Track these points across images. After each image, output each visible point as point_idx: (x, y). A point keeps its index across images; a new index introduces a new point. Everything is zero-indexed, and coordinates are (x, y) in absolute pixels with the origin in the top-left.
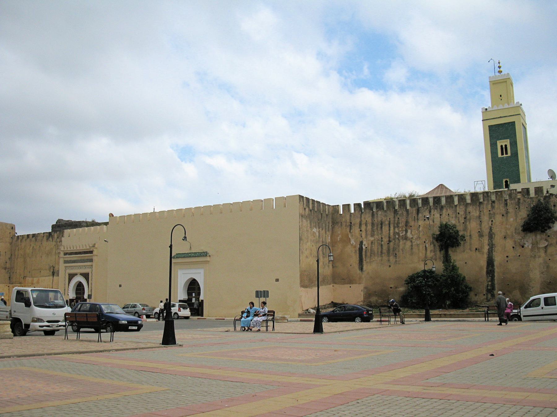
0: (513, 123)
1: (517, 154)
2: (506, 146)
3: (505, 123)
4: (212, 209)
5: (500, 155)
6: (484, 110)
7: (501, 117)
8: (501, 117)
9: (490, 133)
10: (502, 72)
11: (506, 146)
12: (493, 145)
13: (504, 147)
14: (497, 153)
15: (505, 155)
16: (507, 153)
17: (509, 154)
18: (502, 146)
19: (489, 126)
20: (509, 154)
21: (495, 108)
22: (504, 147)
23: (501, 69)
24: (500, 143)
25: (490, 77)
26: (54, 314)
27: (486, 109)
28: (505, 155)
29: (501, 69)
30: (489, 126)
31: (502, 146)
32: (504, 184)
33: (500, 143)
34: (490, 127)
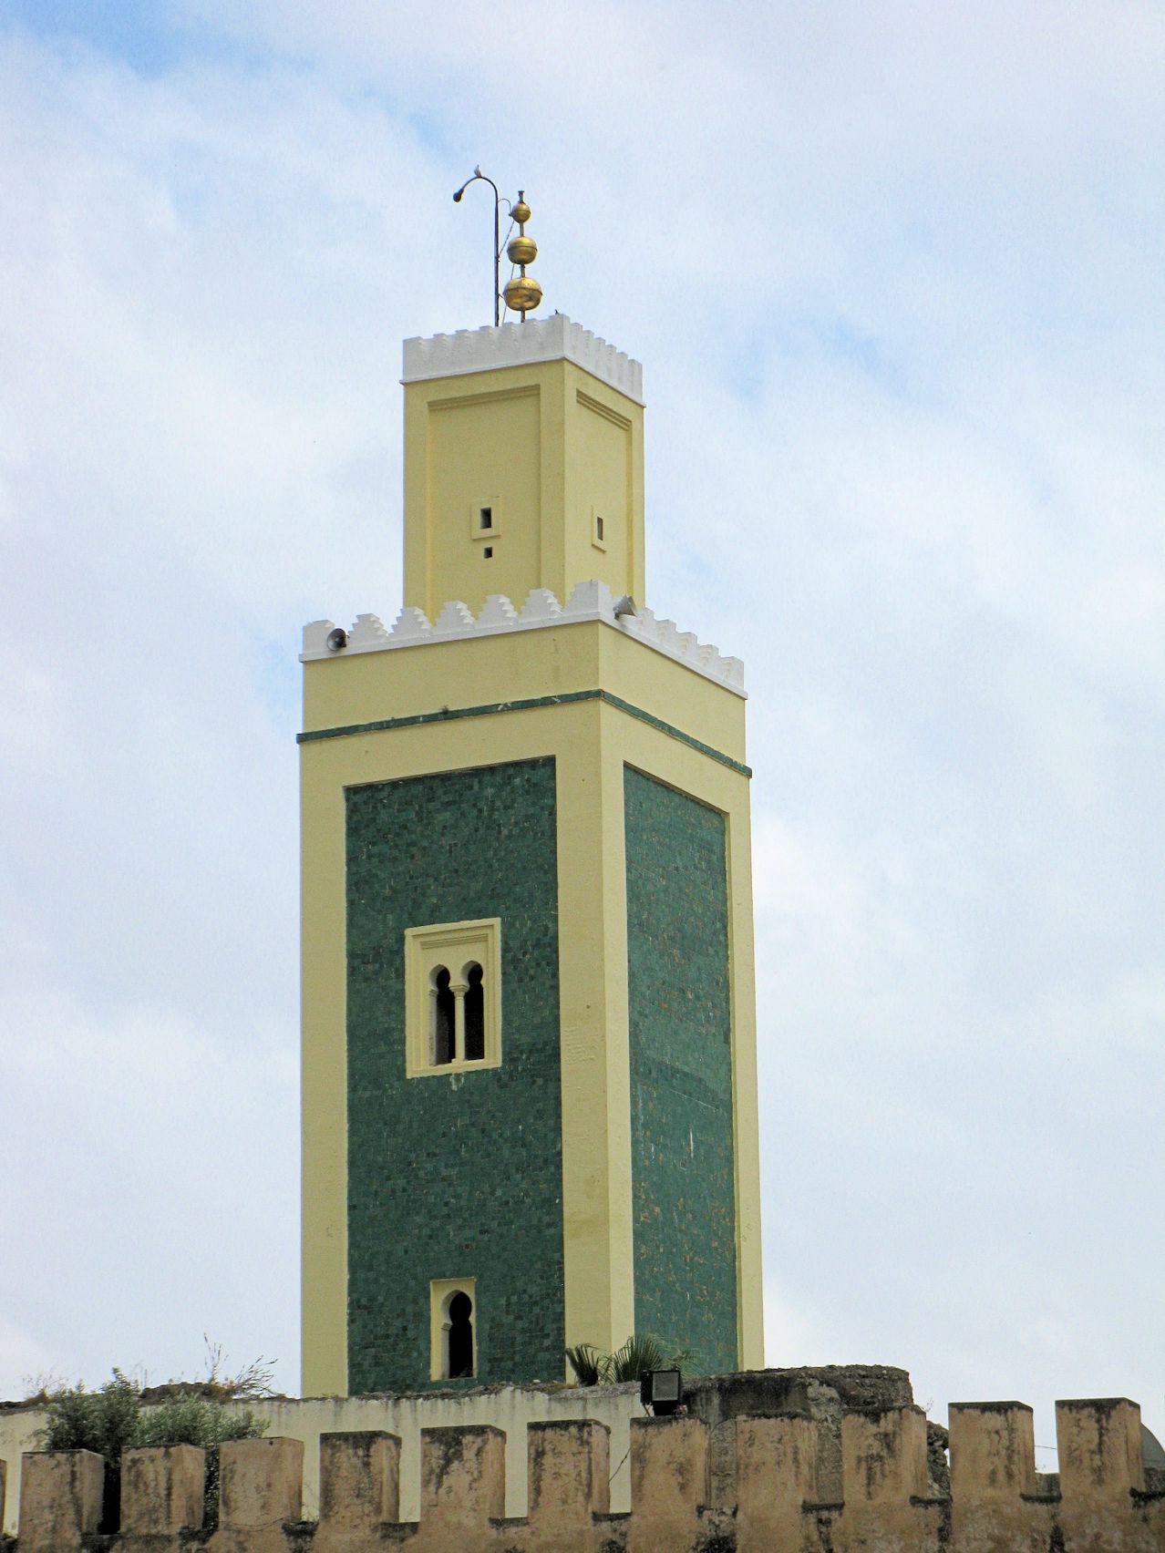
0: (532, 781)
1: (556, 1056)
2: (475, 973)
3: (477, 772)
4: (358, 1065)
5: (419, 1060)
6: (322, 649)
7: (447, 715)
8: (447, 715)
9: (352, 859)
10: (534, 297)
11: (475, 973)
12: (372, 969)
13: (458, 983)
14: (394, 1038)
15: (460, 1064)
16: (475, 1050)
17: (493, 1057)
18: (442, 977)
19: (351, 791)
20: (493, 1057)
21: (426, 631)
22: (458, 983)
23: (535, 274)
24: (427, 953)
25: (410, 345)
26: (600, 1223)
27: (340, 639)
28: (460, 1064)
29: (535, 274)
30: (351, 791)
31: (442, 977)
32: (439, 1320)
33: (427, 953)
34: (363, 800)
